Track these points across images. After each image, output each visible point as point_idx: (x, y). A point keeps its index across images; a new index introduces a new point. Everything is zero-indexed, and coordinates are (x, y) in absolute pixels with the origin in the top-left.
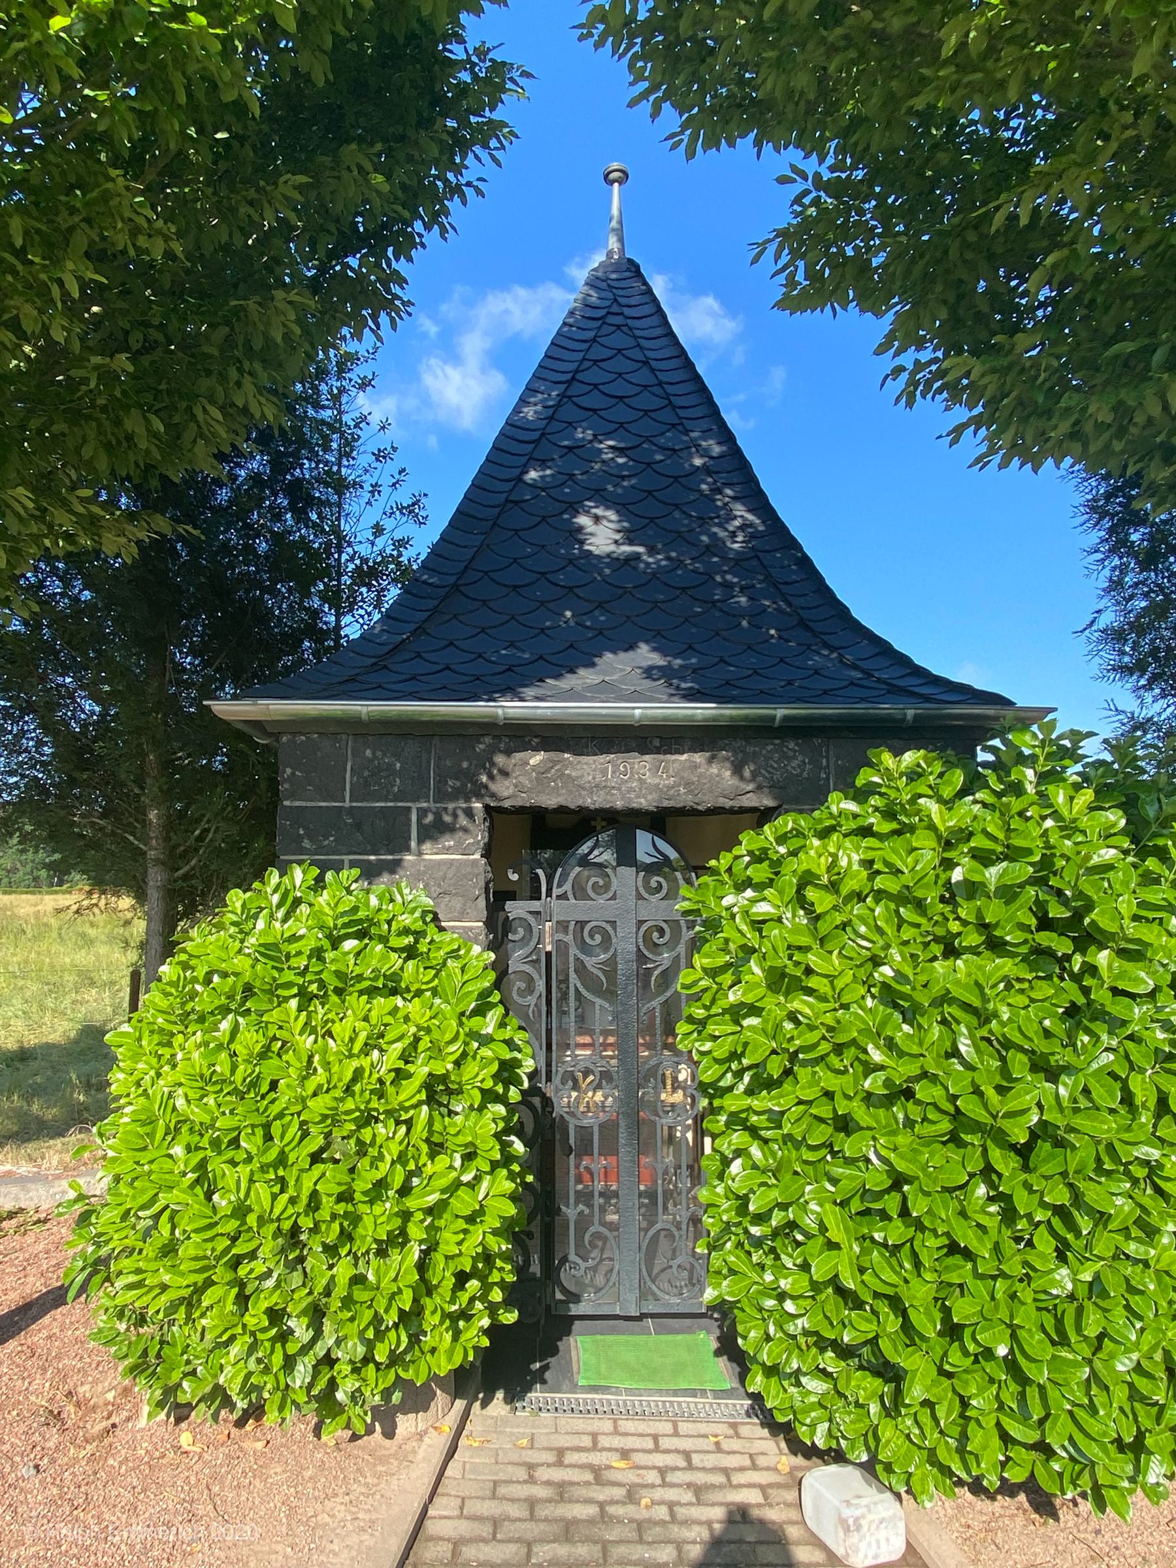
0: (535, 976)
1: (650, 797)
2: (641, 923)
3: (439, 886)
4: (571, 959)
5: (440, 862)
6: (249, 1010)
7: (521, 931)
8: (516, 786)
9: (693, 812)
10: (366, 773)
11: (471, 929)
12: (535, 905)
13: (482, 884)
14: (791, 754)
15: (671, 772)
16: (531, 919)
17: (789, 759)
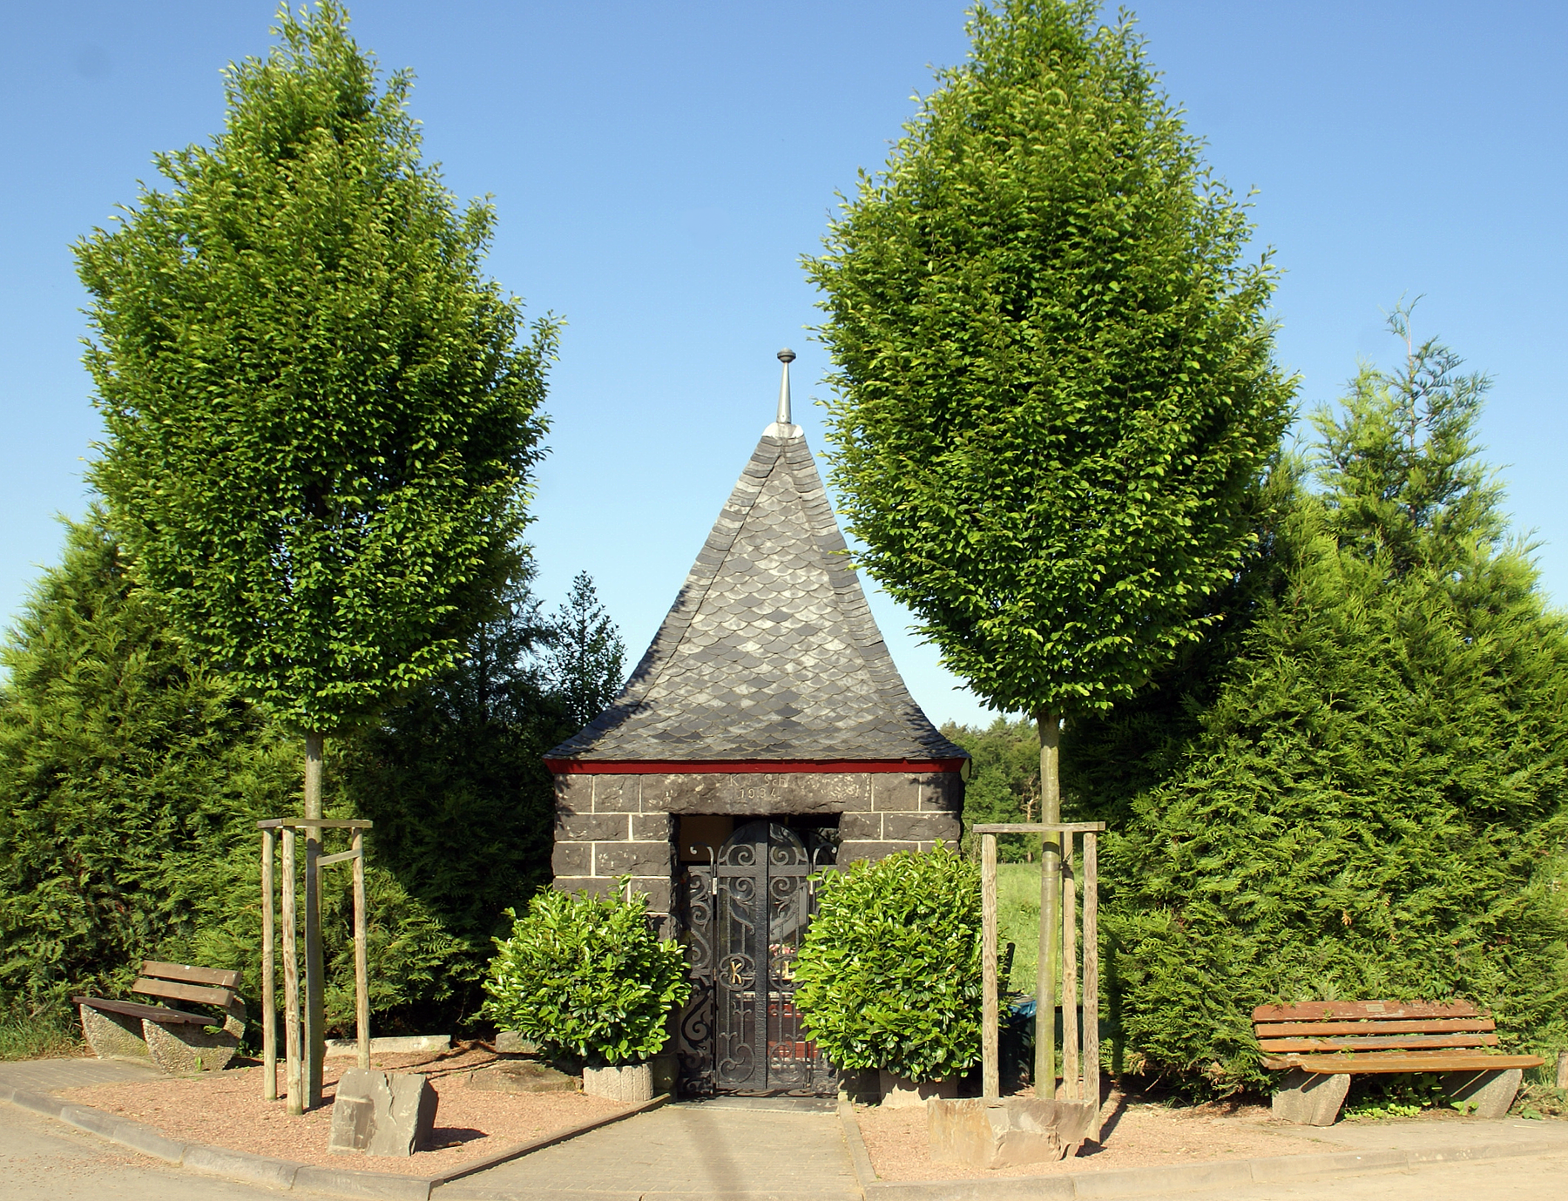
12: (707, 868)
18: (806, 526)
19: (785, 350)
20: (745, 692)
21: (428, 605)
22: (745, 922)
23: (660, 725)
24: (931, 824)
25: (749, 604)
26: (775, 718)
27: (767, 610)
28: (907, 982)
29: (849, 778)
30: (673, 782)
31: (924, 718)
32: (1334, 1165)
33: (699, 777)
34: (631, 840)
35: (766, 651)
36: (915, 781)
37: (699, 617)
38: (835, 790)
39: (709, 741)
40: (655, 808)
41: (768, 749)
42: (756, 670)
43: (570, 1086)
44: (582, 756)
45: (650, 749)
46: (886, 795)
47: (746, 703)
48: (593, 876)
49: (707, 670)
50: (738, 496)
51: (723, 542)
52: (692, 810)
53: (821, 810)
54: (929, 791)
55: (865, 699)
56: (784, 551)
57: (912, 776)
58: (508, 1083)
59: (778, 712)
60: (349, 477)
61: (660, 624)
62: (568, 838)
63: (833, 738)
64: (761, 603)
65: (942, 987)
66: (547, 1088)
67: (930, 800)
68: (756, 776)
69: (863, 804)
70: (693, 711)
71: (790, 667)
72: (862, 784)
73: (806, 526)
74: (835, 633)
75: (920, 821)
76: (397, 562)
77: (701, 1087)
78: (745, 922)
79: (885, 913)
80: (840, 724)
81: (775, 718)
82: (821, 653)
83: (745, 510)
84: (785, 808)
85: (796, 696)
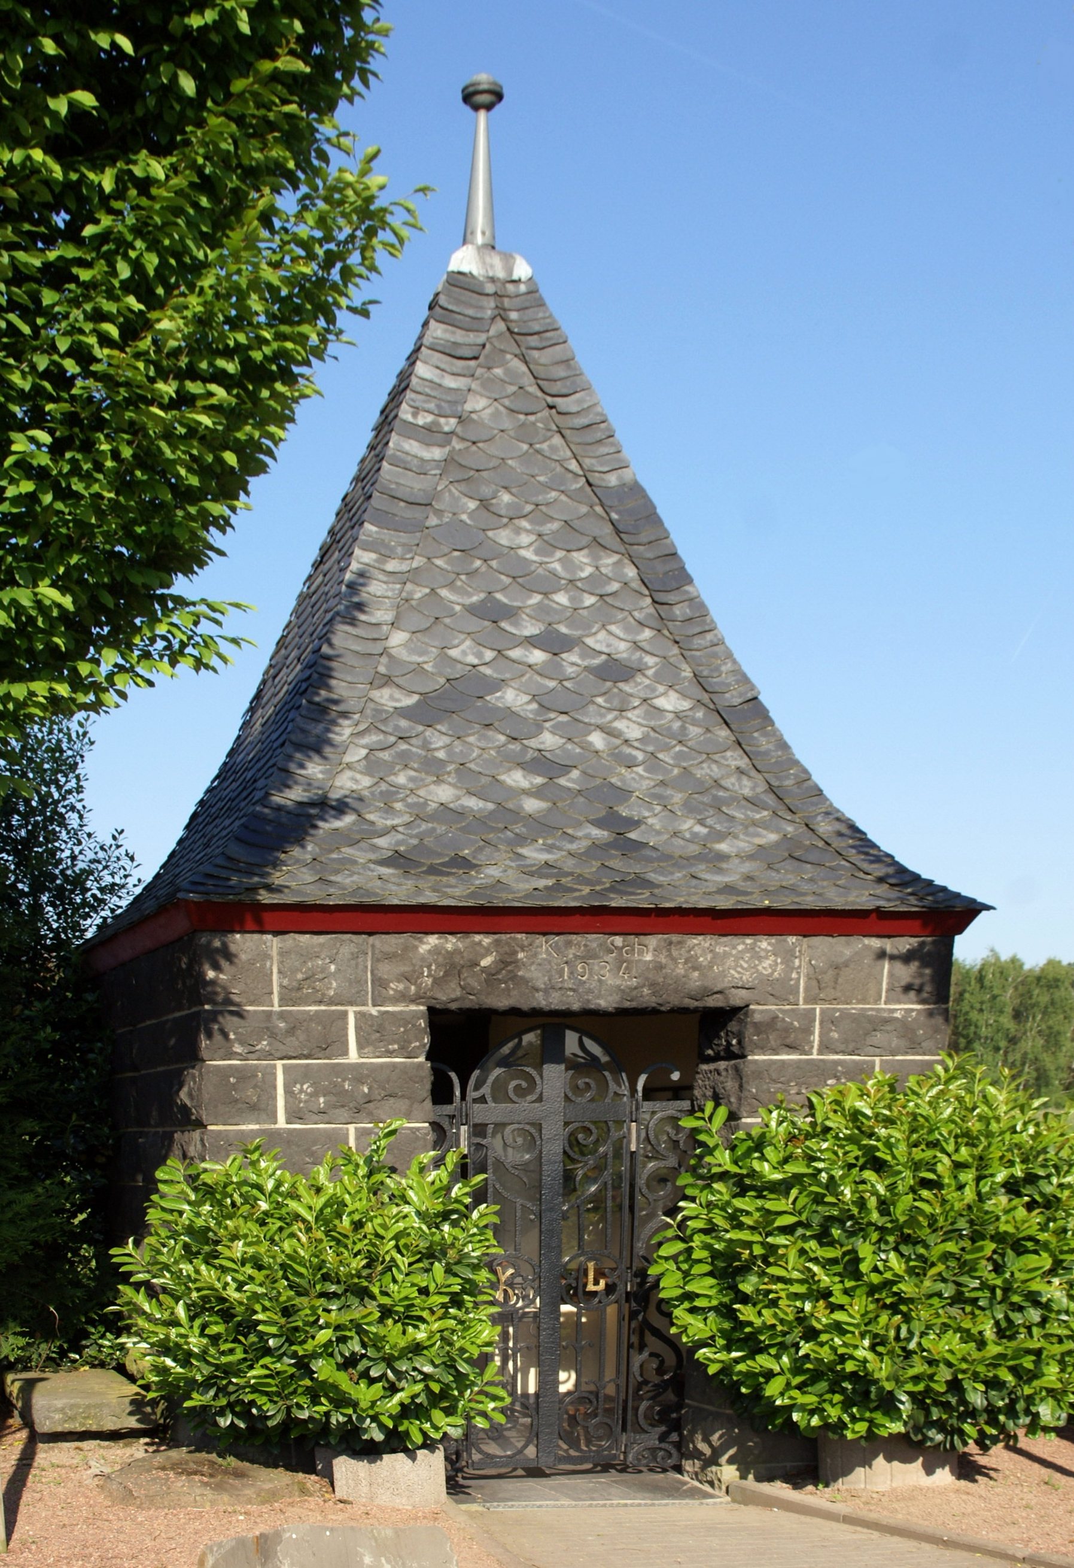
1: (610, 999)
3: (384, 1089)
5: (382, 1066)
6: (931, 1305)
9: (654, 1012)
10: (300, 976)
11: (418, 1129)
14: (763, 954)
15: (634, 972)
17: (760, 959)
18: (573, 465)
19: (483, 78)
23: (382, 842)
27: (531, 629)
29: (765, 944)
30: (436, 951)
32: (992, 1473)
33: (486, 940)
34: (353, 1055)
36: (882, 955)
38: (738, 966)
39: (494, 872)
40: (402, 997)
42: (533, 743)
44: (265, 897)
45: (399, 890)
47: (532, 805)
52: (471, 1002)
53: (712, 1002)
54: (906, 973)
55: (753, 802)
56: (539, 513)
57: (875, 943)
59: (598, 823)
63: (721, 871)
64: (511, 613)
67: (908, 988)
68: (594, 940)
69: (782, 991)
71: (597, 740)
72: (789, 956)
74: (669, 679)
80: (723, 847)
82: (647, 715)
84: (647, 998)
85: (624, 793)
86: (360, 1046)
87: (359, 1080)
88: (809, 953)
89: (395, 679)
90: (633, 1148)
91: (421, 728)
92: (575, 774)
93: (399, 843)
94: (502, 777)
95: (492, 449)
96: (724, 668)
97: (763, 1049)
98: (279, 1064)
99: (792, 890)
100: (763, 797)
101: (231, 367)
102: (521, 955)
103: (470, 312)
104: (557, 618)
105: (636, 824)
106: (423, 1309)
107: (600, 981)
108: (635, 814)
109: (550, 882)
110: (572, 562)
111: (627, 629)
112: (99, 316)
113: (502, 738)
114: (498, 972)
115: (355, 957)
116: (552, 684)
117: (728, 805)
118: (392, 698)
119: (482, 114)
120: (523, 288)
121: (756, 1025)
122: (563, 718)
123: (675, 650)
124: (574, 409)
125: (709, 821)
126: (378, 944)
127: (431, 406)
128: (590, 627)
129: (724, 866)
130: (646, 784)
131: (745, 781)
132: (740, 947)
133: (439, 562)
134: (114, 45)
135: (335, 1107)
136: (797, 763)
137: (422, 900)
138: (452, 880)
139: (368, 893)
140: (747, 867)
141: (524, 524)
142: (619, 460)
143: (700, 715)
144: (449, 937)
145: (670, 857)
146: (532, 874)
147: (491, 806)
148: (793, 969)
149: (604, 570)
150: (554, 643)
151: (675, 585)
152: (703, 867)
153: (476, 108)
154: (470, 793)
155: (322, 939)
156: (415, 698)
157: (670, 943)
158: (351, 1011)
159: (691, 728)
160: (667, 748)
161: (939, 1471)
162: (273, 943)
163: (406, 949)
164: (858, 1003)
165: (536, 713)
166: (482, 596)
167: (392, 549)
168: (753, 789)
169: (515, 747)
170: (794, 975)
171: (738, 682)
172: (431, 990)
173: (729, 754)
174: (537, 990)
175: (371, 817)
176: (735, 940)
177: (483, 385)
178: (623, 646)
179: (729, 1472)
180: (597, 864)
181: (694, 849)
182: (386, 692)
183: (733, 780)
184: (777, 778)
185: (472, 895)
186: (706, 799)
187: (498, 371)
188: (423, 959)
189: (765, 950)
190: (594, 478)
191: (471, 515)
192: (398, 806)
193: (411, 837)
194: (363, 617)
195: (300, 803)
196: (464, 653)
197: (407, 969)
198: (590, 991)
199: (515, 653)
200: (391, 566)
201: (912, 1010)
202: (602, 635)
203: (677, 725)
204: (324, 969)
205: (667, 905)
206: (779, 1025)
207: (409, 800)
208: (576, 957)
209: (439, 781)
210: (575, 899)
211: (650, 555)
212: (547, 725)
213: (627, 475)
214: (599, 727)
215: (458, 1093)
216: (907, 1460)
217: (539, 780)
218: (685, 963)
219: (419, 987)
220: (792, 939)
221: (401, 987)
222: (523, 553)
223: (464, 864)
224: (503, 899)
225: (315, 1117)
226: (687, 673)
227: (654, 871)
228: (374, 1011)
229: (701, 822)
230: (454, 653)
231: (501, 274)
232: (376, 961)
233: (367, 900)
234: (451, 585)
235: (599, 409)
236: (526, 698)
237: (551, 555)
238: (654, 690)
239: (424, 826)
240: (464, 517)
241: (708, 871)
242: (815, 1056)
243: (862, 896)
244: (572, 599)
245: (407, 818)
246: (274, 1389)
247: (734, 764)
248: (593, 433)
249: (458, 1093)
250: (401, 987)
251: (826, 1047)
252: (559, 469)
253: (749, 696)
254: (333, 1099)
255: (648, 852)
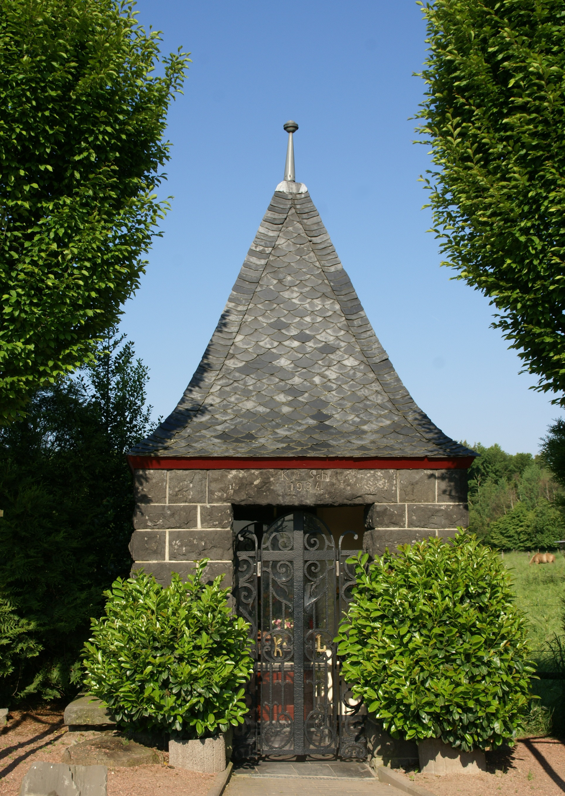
0: (253, 589)
2: (306, 561)
3: (211, 543)
4: (271, 580)
5: (211, 532)
7: (245, 566)
8: (247, 495)
9: (331, 506)
10: (177, 489)
11: (226, 563)
12: (252, 553)
13: (231, 542)
15: (321, 487)
16: (251, 561)
18: (317, 264)
19: (291, 122)
20: (284, 400)
21: (80, 307)
22: (284, 602)
23: (219, 428)
24: (447, 514)
25: (279, 326)
26: (312, 422)
27: (294, 332)
28: (468, 657)
29: (379, 473)
30: (235, 477)
31: (430, 422)
33: (257, 472)
34: (199, 527)
35: (296, 366)
37: (239, 338)
38: (369, 484)
39: (262, 441)
40: (220, 499)
41: (312, 448)
42: (290, 382)
43: (155, 760)
44: (162, 453)
45: (218, 449)
46: (410, 487)
47: (286, 410)
48: (167, 560)
49: (250, 381)
50: (260, 238)
51: (253, 275)
52: (251, 501)
53: (357, 501)
54: (444, 485)
55: (382, 406)
56: (301, 284)
57: (429, 472)
58: (105, 758)
59: (313, 417)
60: (20, 181)
61: (208, 342)
62: (146, 527)
63: (362, 439)
64: (287, 326)
65: (496, 660)
66: (137, 762)
67: (444, 492)
68: (303, 472)
69: (389, 496)
70: (243, 416)
72: (390, 479)
73: (317, 264)
74: (350, 352)
75: (438, 511)
76: (58, 264)
77: (246, 753)
78: (284, 602)
79: (442, 592)
80: (365, 427)
81: (312, 422)
82: (340, 368)
83: (269, 250)
84: (328, 499)
85: (325, 404)
86: (202, 523)
87: (201, 539)
88: (400, 478)
89: (238, 356)
90: (338, 574)
91: (244, 376)
92: (306, 395)
93: (226, 428)
94: (275, 397)
95: (286, 260)
96: (374, 347)
97: (382, 525)
98: (167, 531)
99: (392, 448)
100: (386, 404)
101: (88, 264)
102: (272, 479)
103: (281, 206)
104: (305, 327)
105: (329, 417)
106: (198, 657)
107: (307, 491)
108: (329, 413)
109: (284, 445)
110: (313, 303)
111: (334, 331)
112: (41, 251)
113: (277, 380)
114: (262, 487)
115: (201, 480)
116: (301, 356)
117: (370, 408)
118: (234, 364)
119: (291, 134)
120: (303, 196)
121: (377, 512)
122: (304, 370)
123: (354, 340)
124: (319, 242)
125: (361, 416)
126: (211, 475)
127: (263, 243)
128: (319, 331)
129: (364, 436)
130: (336, 399)
131: (380, 397)
132: (369, 475)
133: (259, 306)
134: (46, 168)
135: (190, 552)
136: (404, 388)
137: (226, 454)
138: (243, 445)
139: (206, 451)
140: (374, 437)
141: (296, 289)
142: (336, 261)
143: (362, 367)
144: (241, 471)
145: (341, 432)
146: (278, 441)
147: (268, 410)
148: (393, 485)
149: (326, 307)
150: (303, 338)
151: (355, 311)
152: (354, 437)
153: (289, 132)
154: (260, 404)
155: (187, 472)
156: (244, 363)
157: (337, 473)
158: (199, 506)
159: (358, 373)
160: (347, 383)
161: (470, 764)
162: (168, 474)
163: (222, 476)
164: (425, 502)
165: (293, 368)
166: (276, 319)
167: (241, 301)
168: (382, 400)
169: (282, 384)
170: (394, 488)
171: (379, 352)
172: (233, 495)
173: (373, 384)
174: (279, 495)
175: (217, 416)
176: (366, 471)
177: (284, 234)
178: (332, 338)
179: (378, 761)
180: (308, 436)
181: (353, 428)
182: (232, 361)
183: (374, 396)
184: (393, 395)
185: (250, 452)
186: (361, 405)
187: (290, 228)
188: (229, 481)
189: (379, 476)
190: (325, 269)
191: (274, 286)
192: (229, 411)
193: (232, 425)
194: (226, 330)
195: (187, 410)
196: (266, 344)
197: (223, 486)
198: (303, 496)
199: (286, 343)
200: (240, 308)
201: (450, 505)
202: (324, 333)
203: (352, 372)
204: (187, 486)
205: (332, 456)
206: (388, 513)
207: (235, 408)
208: (296, 480)
209: (248, 400)
210: (293, 453)
211: (345, 300)
212: (297, 373)
213: (339, 267)
214: (318, 374)
215: (256, 545)
216: (453, 757)
217: (290, 398)
218: (344, 482)
219: (227, 494)
220: (392, 471)
221: (220, 494)
222: (294, 300)
223: (251, 437)
224: (265, 454)
225: (182, 557)
226: (358, 349)
227: (333, 439)
228: (208, 506)
229: (357, 416)
230: (261, 344)
231: (295, 191)
232: (210, 482)
233: (203, 455)
234: (263, 315)
235: (329, 241)
236: (289, 362)
237: (305, 301)
238: (343, 357)
239: (239, 420)
240: (271, 287)
241: (357, 439)
242: (406, 528)
243: (420, 451)
244: (312, 319)
245: (232, 416)
246: (134, 699)
247: (375, 389)
248: (326, 251)
249: (256, 545)
250: (220, 494)
251: (411, 524)
252: (312, 266)
253: (384, 358)
254: (189, 548)
255: (332, 430)
